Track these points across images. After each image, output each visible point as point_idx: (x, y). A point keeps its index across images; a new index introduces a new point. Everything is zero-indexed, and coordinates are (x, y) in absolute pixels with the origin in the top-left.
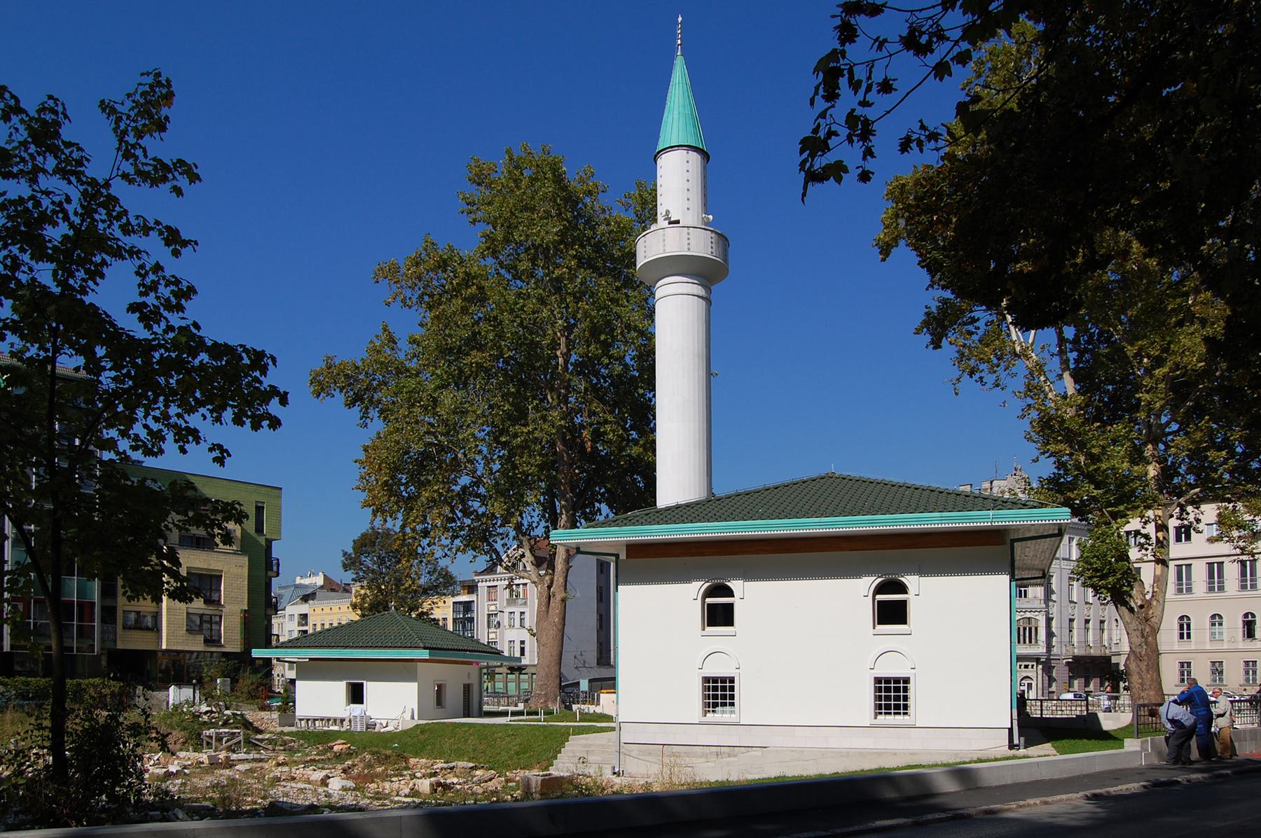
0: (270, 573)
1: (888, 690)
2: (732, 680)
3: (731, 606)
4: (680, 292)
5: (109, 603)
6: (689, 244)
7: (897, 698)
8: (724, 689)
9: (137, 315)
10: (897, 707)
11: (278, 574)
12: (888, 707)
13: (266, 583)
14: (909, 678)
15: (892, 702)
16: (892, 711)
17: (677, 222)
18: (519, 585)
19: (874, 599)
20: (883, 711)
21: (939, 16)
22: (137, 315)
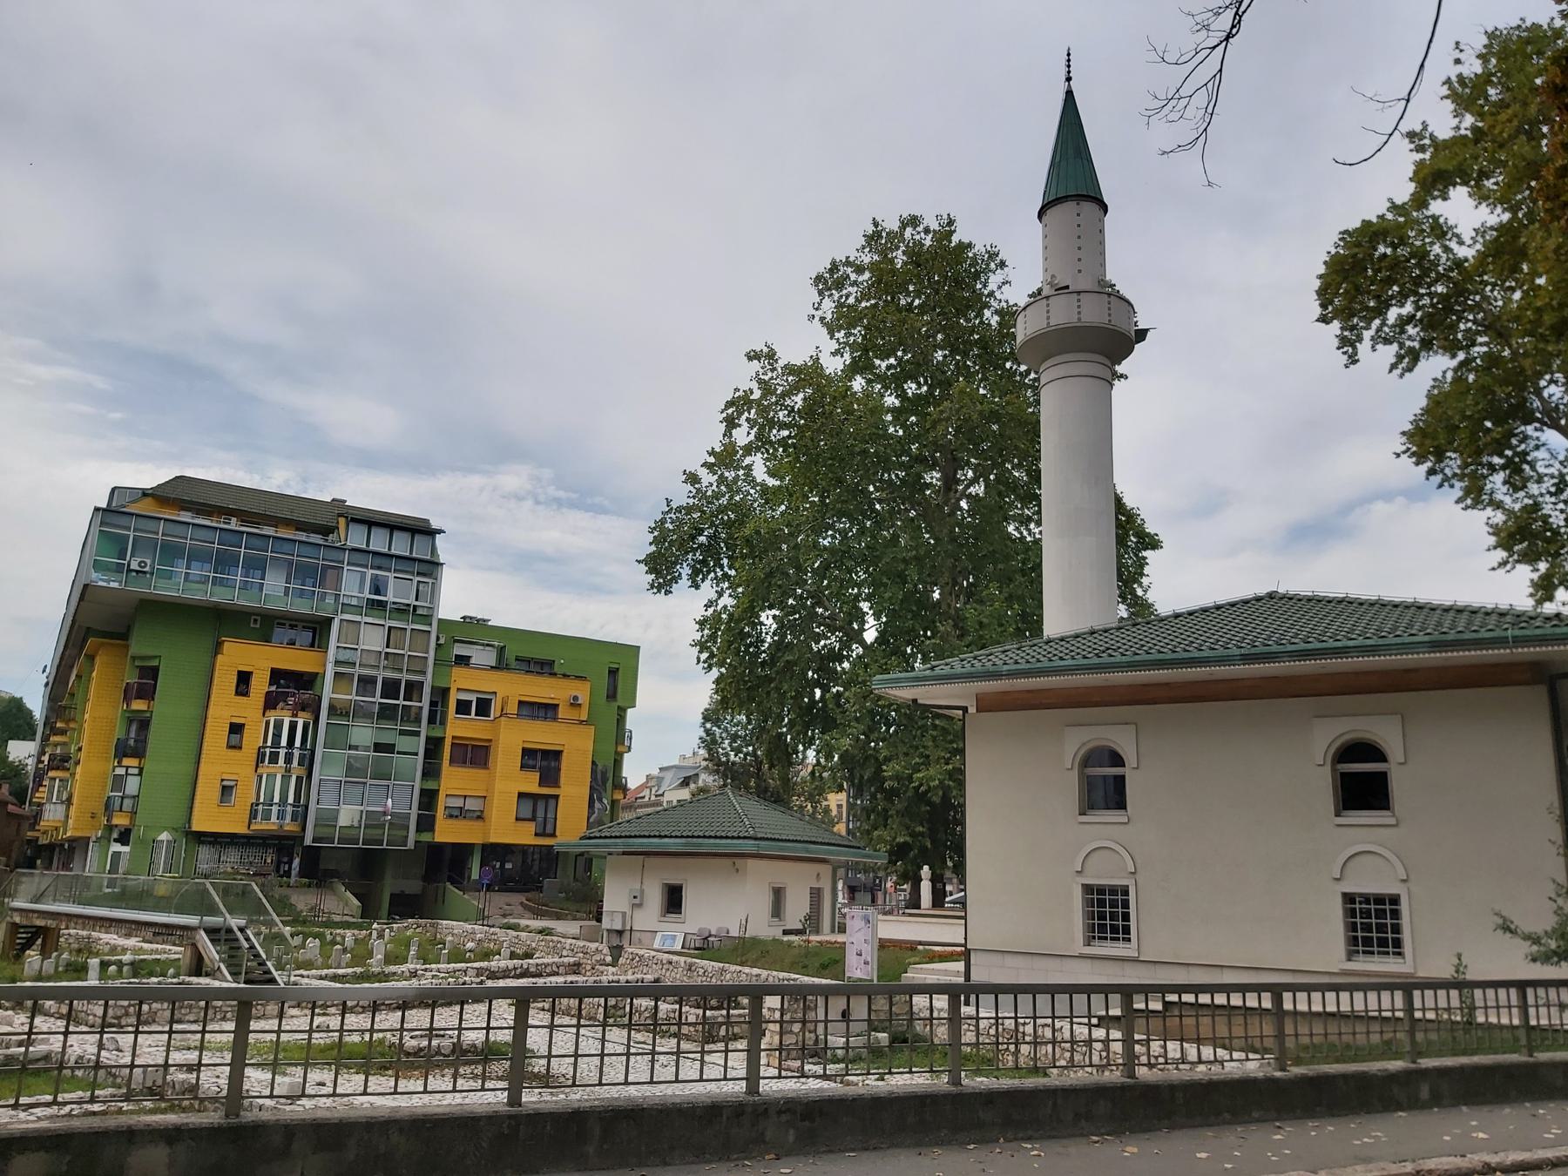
0: (620, 749)
1: (1114, 904)
2: (1395, 900)
3: (1383, 776)
4: (1091, 373)
5: (430, 785)
6: (1109, 309)
7: (1381, 928)
8: (1381, 914)
9: (1358, 344)
10: (1383, 943)
11: (629, 749)
12: (1367, 942)
13: (615, 760)
14: (1399, 895)
15: (1374, 935)
16: (1376, 949)
17: (1067, 287)
18: (54, 779)
19: (1334, 770)
20: (1360, 948)
21: (1210, 21)
22: (1358, 344)
